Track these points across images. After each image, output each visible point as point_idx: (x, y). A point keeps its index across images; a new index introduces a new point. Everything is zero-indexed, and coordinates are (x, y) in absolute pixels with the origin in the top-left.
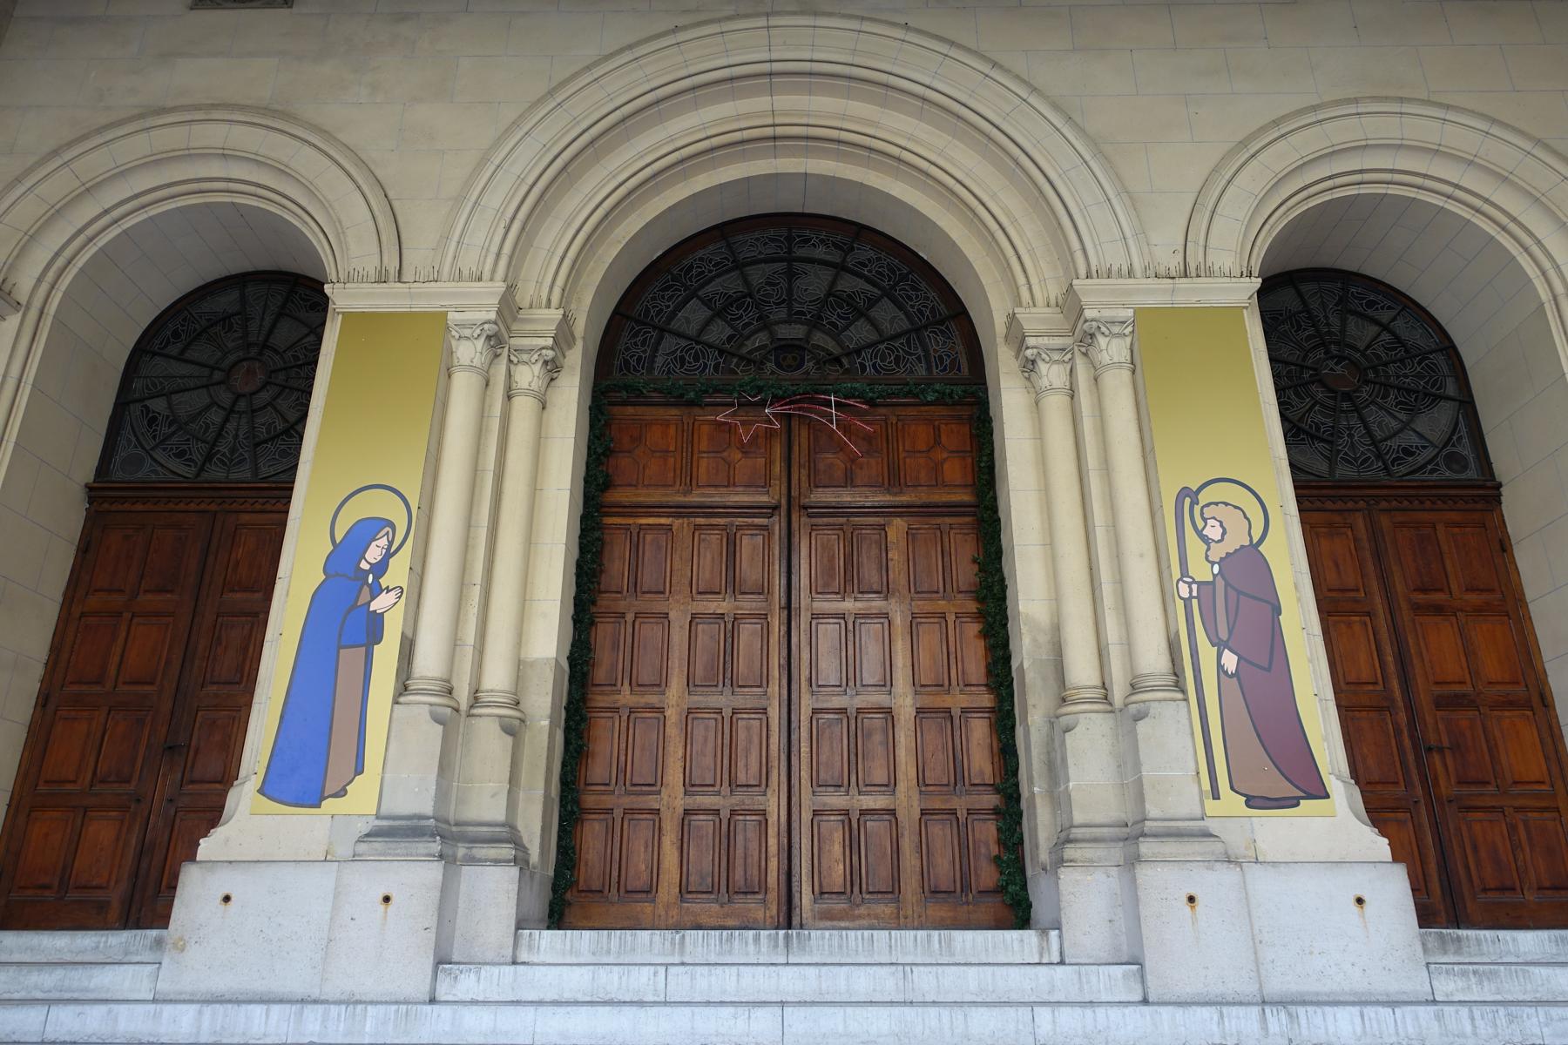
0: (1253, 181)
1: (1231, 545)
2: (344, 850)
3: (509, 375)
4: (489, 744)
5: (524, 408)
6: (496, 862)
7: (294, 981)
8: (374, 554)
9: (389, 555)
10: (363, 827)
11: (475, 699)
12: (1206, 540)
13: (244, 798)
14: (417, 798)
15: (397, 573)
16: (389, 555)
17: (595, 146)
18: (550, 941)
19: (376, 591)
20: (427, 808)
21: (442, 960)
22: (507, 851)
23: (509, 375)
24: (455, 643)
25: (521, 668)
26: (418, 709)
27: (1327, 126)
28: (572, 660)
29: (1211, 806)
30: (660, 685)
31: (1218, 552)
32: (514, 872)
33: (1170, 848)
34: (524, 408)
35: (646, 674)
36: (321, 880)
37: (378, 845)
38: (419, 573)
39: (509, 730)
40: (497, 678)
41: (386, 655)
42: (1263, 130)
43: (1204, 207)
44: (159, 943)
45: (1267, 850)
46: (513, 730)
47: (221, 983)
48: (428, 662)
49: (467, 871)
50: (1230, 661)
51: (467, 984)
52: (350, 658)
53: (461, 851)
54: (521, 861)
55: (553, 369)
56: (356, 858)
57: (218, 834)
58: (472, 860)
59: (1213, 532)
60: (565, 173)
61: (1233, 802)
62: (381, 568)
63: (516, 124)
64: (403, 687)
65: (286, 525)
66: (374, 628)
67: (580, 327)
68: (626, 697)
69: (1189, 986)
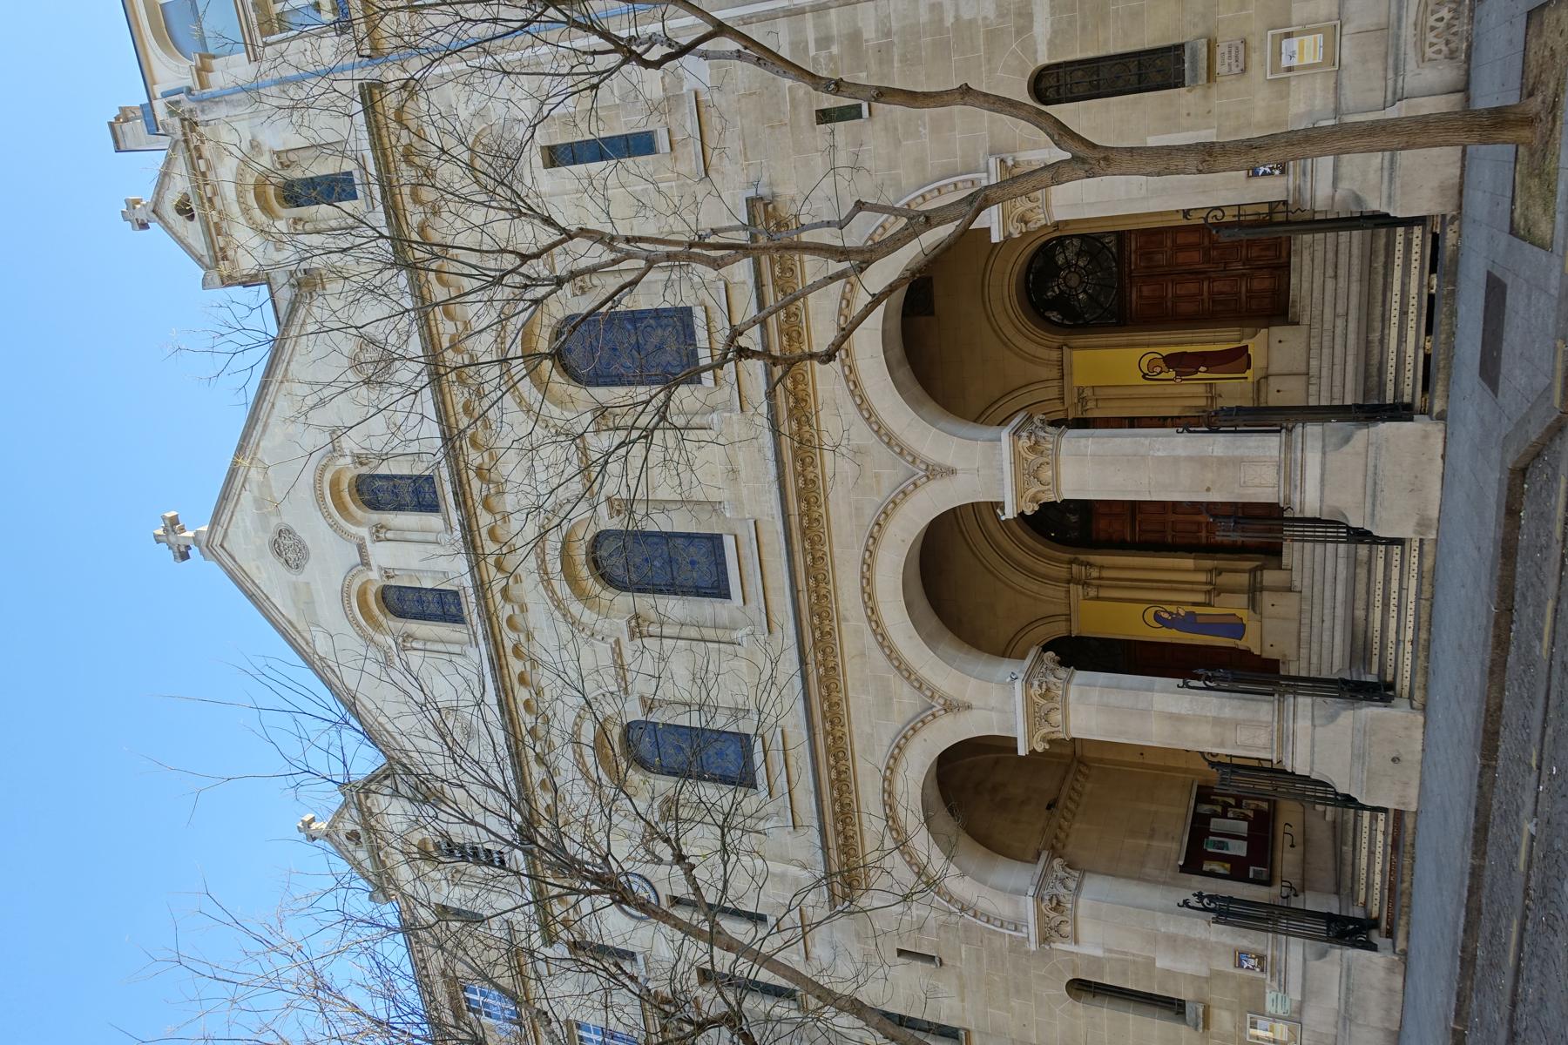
0: (1020, 341)
1: (1163, 365)
2: (1258, 617)
3: (1094, 579)
4: (1225, 579)
5: (1105, 574)
6: (1262, 576)
7: (1295, 626)
8: (1166, 616)
9: (1166, 611)
10: (1252, 613)
11: (1211, 583)
12: (1160, 373)
13: (1242, 644)
14: (1243, 599)
15: (1172, 609)
16: (1166, 611)
17: (1006, 557)
18: (1285, 561)
19: (1178, 614)
20: (1246, 596)
21: (1290, 590)
22: (1259, 573)
23: (1094, 579)
24: (1192, 591)
25: (1197, 570)
26: (1216, 600)
27: (1001, 325)
28: (1190, 552)
29: (1250, 380)
30: (1199, 524)
31: (1165, 369)
32: (1265, 571)
33: (1263, 395)
34: (1105, 574)
35: (1194, 528)
36: (1266, 622)
37: (1257, 608)
38: (1171, 603)
39: (1220, 574)
40: (1202, 577)
41: (1198, 610)
42: (998, 336)
43: (1034, 359)
44: (1283, 663)
45: (1263, 364)
46: (1220, 572)
47: (1295, 644)
48: (1200, 598)
49: (1265, 583)
50: (1202, 369)
51: (1297, 583)
52: (1199, 620)
53: (1258, 585)
54: (1262, 568)
55: (1089, 564)
56: (1261, 614)
57: (1252, 650)
58: (1261, 581)
59: (1158, 370)
60: (1019, 566)
61: (1249, 373)
62: (1170, 613)
63: (1004, 583)
64: (1209, 605)
65: (1129, 641)
66: (1191, 614)
67: (1072, 556)
68: (1204, 534)
69: (1304, 365)
